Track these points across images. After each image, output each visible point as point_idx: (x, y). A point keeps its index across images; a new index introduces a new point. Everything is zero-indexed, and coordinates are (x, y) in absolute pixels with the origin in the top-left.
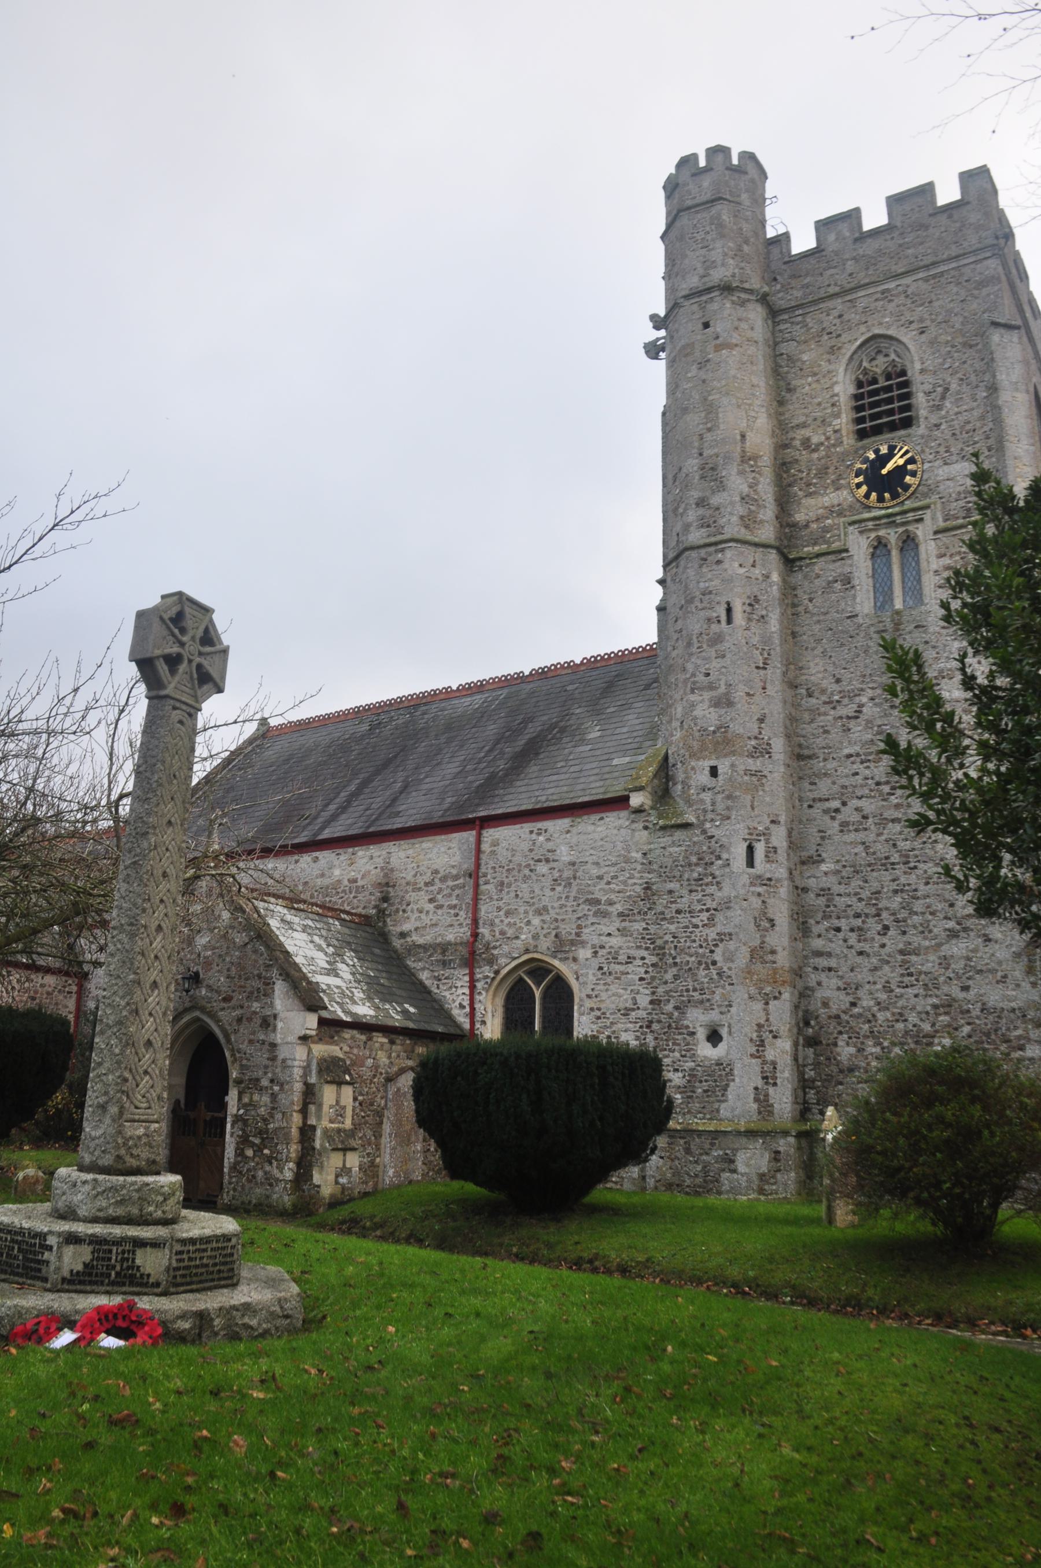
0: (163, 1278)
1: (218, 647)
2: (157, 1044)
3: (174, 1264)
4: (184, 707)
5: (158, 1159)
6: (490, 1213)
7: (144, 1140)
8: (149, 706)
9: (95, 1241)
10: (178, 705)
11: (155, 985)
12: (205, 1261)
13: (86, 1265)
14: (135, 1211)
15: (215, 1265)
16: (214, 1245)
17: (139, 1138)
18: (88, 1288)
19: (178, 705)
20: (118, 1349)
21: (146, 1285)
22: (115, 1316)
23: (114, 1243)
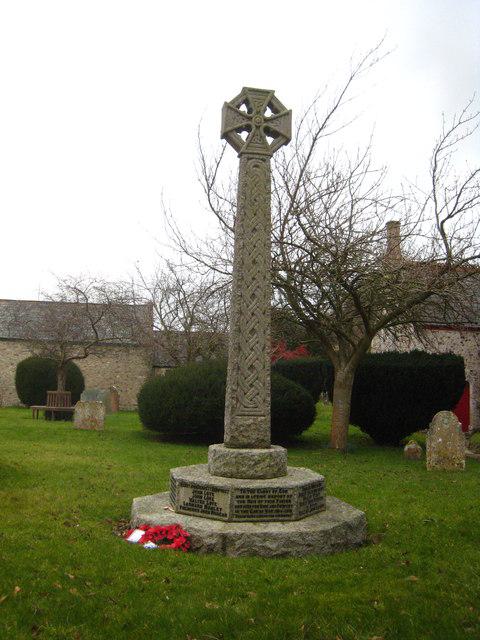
0: (227, 511)
1: (282, 113)
2: (258, 365)
3: (236, 503)
4: (257, 156)
5: (266, 439)
6: (146, 438)
7: (253, 427)
8: (242, 167)
9: (195, 487)
10: (251, 156)
11: (253, 331)
12: (263, 503)
13: (190, 500)
14: (234, 470)
15: (273, 506)
16: (256, 494)
17: (249, 426)
18: (192, 513)
19: (251, 156)
20: (154, 550)
21: (219, 514)
22: (167, 532)
23: (203, 488)
